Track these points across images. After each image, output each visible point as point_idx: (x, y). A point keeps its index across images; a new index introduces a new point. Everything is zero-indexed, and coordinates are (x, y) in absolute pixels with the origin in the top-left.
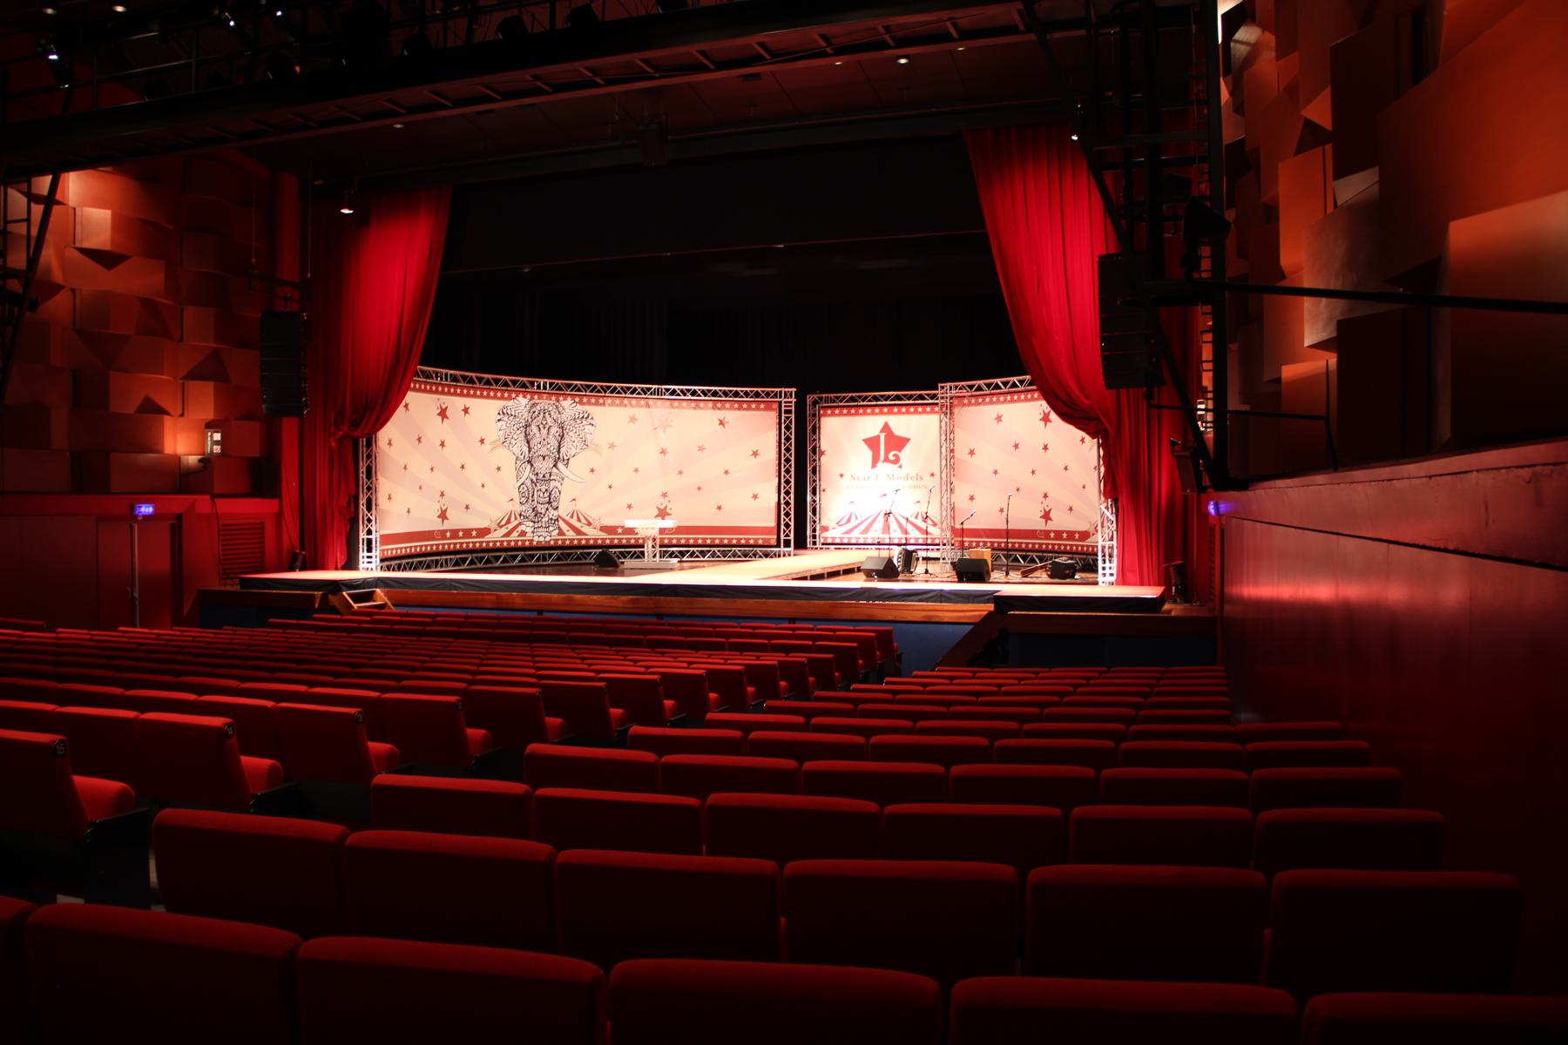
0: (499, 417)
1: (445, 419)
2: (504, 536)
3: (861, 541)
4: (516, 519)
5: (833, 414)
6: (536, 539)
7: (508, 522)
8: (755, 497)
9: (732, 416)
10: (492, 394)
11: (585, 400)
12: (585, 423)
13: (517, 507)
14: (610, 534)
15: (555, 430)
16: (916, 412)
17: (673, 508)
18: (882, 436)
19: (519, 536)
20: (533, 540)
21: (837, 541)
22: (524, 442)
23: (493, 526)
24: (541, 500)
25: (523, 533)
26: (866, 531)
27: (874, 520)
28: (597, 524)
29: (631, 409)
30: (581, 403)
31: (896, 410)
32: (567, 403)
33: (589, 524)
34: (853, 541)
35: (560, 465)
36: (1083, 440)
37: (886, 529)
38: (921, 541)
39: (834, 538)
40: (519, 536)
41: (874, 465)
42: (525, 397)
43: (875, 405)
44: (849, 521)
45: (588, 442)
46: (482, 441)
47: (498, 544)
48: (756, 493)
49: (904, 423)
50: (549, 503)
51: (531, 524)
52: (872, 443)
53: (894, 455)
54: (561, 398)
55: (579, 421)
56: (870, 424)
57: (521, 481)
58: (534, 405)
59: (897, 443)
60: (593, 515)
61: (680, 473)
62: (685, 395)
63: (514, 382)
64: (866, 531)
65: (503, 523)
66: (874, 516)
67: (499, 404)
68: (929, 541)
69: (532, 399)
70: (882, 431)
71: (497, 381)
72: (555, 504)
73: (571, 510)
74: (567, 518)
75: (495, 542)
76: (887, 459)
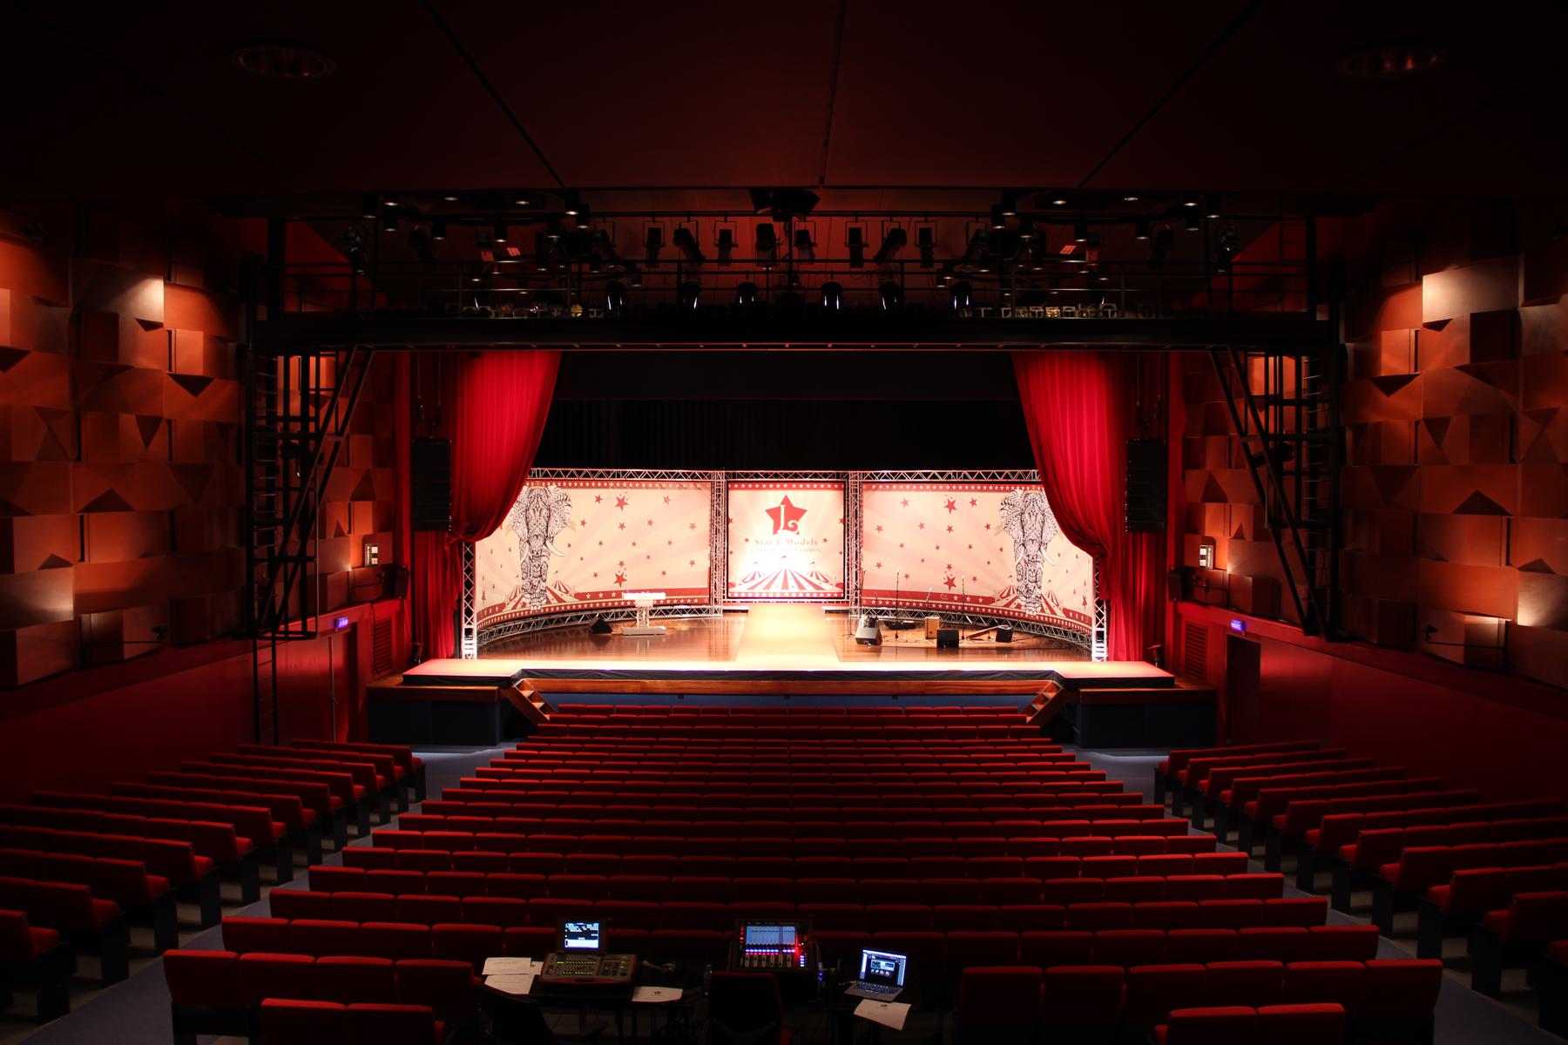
0: (1002, 507)
1: (624, 507)
2: (1004, 606)
3: (764, 595)
4: (1014, 592)
5: (740, 488)
6: (1028, 612)
7: (1008, 595)
8: (692, 563)
9: (963, 497)
10: (565, 484)
11: (625, 484)
12: (564, 504)
13: (520, 583)
14: (581, 600)
15: (545, 512)
16: (812, 488)
17: (912, 578)
18: (783, 507)
19: (1016, 608)
20: (529, 610)
21: (743, 595)
22: (1020, 528)
23: (997, 597)
24: (1031, 579)
25: (1019, 606)
26: (767, 587)
27: (775, 578)
28: (572, 592)
29: (661, 491)
30: (562, 487)
31: (794, 486)
32: (552, 488)
33: (567, 592)
34: (757, 595)
35: (548, 542)
36: (667, 500)
37: (785, 586)
38: (815, 595)
39: (740, 593)
40: (1016, 608)
41: (775, 531)
42: (1021, 489)
43: (777, 482)
44: (753, 579)
45: (567, 521)
46: (988, 527)
47: (558, 609)
48: (619, 563)
49: (800, 497)
50: (541, 576)
51: (1025, 599)
52: (773, 513)
53: (793, 524)
54: (549, 484)
55: (560, 503)
56: (773, 497)
57: (523, 559)
58: (532, 491)
59: (795, 513)
60: (569, 584)
61: (634, 544)
62: (686, 477)
63: (553, 472)
64: (767, 587)
65: (1004, 595)
66: (774, 575)
67: (1002, 495)
68: (822, 595)
69: (1025, 490)
70: (783, 503)
71: (566, 473)
72: (544, 577)
73: (554, 581)
74: (552, 588)
75: (998, 610)
76: (786, 527)
